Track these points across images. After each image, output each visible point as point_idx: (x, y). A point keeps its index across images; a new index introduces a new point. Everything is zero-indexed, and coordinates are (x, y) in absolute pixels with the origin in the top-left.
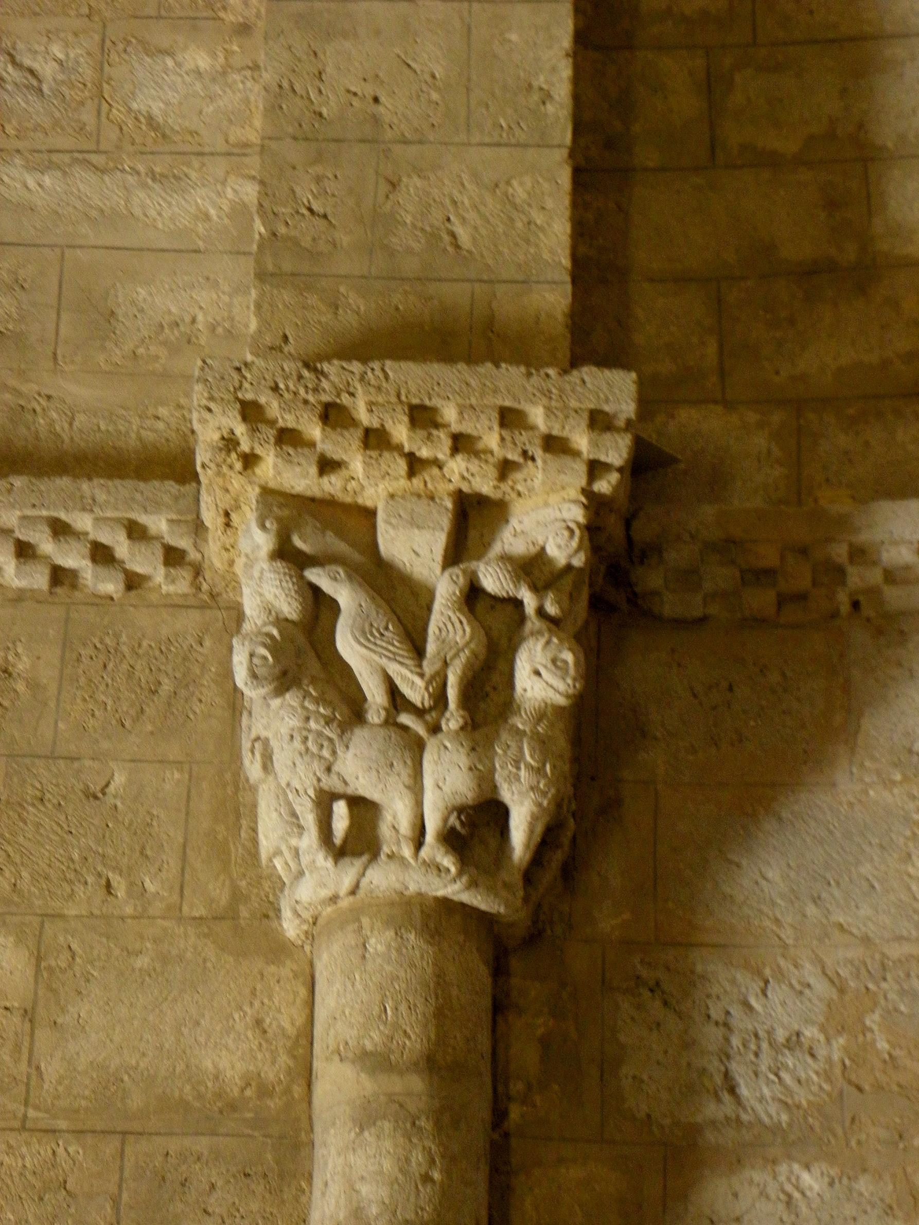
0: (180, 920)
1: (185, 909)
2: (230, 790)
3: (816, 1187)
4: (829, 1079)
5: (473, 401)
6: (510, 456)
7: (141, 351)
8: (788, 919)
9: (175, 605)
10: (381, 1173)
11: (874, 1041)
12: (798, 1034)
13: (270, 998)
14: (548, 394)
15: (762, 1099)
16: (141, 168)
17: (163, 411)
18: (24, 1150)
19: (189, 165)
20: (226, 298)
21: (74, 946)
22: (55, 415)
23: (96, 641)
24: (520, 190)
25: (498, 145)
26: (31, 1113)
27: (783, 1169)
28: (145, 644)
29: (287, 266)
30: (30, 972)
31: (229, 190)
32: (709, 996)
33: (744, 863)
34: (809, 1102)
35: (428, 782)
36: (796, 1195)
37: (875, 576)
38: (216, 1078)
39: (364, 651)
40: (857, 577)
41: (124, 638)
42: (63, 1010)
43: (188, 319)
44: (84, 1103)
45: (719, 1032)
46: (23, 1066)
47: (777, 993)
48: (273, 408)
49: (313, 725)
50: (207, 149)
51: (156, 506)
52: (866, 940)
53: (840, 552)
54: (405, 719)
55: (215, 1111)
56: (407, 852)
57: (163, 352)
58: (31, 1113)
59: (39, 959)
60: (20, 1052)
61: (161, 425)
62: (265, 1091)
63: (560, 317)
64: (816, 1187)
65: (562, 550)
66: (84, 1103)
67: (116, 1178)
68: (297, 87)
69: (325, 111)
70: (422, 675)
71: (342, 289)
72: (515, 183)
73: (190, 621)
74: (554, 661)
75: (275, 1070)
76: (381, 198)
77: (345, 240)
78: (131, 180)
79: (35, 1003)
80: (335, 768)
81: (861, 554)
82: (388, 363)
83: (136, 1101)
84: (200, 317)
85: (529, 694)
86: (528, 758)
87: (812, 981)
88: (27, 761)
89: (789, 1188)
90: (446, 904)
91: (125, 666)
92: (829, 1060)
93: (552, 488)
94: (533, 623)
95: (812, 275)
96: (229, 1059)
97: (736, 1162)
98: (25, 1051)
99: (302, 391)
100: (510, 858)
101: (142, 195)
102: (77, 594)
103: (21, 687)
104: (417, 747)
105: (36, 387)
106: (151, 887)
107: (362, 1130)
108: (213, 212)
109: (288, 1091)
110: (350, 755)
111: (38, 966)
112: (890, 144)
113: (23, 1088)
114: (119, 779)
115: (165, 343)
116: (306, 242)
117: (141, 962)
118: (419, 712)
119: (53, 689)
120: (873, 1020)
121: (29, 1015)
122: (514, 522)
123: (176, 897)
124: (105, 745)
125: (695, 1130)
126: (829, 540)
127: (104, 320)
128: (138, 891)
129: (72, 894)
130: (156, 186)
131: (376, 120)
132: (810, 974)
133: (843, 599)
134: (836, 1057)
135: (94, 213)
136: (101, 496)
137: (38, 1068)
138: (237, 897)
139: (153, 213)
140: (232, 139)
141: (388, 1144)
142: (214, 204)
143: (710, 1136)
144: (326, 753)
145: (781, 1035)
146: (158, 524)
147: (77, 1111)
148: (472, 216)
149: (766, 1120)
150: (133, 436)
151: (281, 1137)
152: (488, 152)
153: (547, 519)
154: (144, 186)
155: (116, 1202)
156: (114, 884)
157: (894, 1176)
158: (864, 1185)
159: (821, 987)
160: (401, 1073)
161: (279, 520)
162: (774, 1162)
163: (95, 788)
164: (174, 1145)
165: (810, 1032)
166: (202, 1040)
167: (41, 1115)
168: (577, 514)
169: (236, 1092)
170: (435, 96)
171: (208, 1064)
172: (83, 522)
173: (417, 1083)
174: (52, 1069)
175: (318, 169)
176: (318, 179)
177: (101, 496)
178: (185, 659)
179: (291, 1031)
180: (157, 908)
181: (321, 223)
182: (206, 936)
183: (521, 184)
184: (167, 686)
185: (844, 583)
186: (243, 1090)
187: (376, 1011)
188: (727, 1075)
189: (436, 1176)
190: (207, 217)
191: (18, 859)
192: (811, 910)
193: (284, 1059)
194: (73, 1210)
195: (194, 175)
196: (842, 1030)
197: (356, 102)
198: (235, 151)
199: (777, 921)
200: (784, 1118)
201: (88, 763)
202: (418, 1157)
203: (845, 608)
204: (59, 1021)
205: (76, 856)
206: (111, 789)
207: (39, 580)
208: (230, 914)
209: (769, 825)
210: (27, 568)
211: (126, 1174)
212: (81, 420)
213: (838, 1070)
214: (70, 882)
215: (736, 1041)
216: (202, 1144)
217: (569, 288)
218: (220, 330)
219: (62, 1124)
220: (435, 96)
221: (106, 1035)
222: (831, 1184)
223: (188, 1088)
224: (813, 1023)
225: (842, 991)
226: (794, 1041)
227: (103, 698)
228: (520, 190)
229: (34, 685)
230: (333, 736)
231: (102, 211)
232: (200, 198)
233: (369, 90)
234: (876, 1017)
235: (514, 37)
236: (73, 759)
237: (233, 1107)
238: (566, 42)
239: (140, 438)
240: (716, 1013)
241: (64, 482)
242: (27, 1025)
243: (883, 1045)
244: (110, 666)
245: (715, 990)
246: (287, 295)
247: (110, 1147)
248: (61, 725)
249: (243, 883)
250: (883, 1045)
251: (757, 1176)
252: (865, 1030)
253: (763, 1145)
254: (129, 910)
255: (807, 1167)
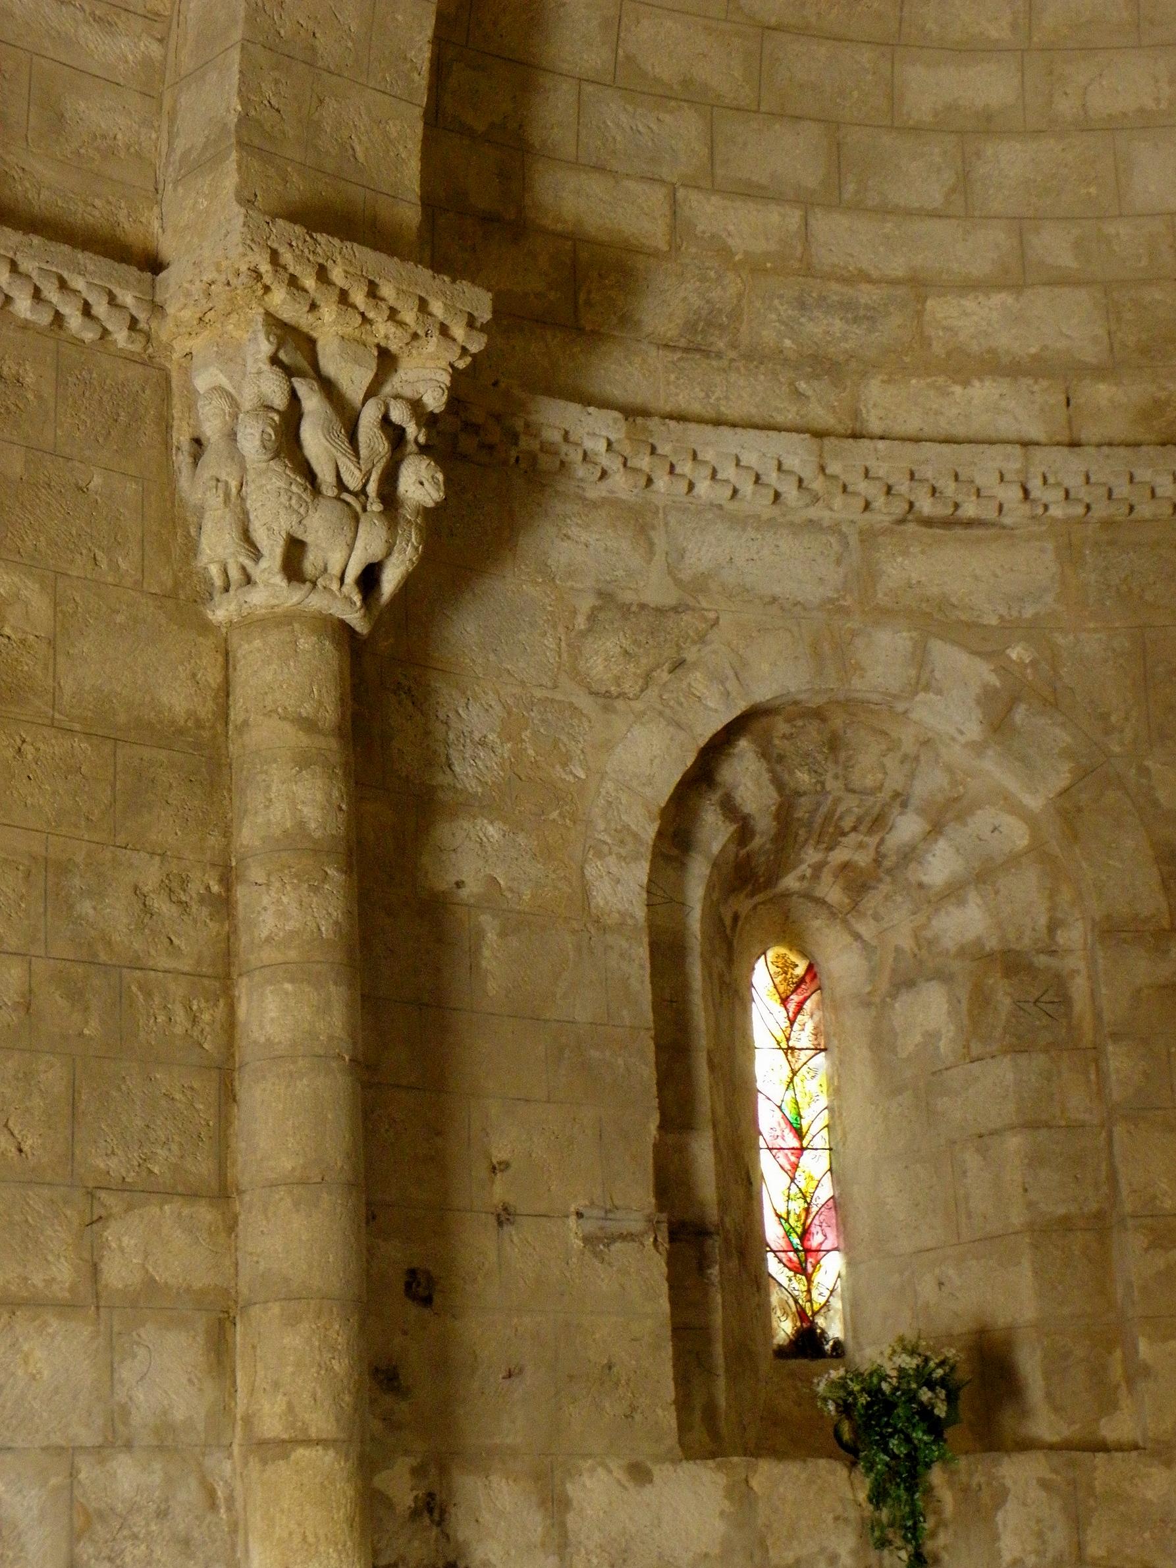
0: (142, 592)
1: (145, 585)
2: (169, 505)
3: (496, 836)
4: (503, 770)
5: (404, 288)
6: (419, 332)
7: (82, 151)
8: (480, 661)
9: (129, 358)
10: (314, 800)
11: (525, 750)
12: (485, 737)
13: (200, 659)
14: (444, 294)
15: (467, 775)
16: (86, 7)
17: (97, 202)
18: (53, 741)
19: (119, 16)
20: (137, 127)
21: (77, 599)
22: (28, 185)
23: (77, 372)
24: (393, 130)
25: (384, 93)
26: (57, 716)
27: (478, 821)
28: (108, 382)
29: (257, 142)
30: (50, 612)
31: (142, 44)
32: (438, 703)
33: (455, 618)
34: (493, 782)
35: (359, 544)
36: (485, 839)
37: (536, 446)
38: (170, 709)
39: (327, 444)
40: (525, 443)
41: (94, 375)
42: (73, 645)
43: (111, 135)
44: (90, 714)
45: (444, 728)
46: (50, 681)
47: (475, 708)
48: (287, 257)
49: (294, 488)
50: (131, 8)
51: (126, 285)
52: (522, 683)
53: (519, 425)
54: (345, 496)
55: (161, 732)
56: (335, 586)
57: (97, 157)
58: (57, 716)
59: (56, 605)
60: (47, 669)
61: (97, 213)
62: (199, 724)
63: (415, 229)
64: (496, 836)
65: (434, 401)
66: (90, 714)
67: (112, 771)
68: (267, 8)
69: (282, 32)
70: (360, 470)
71: (289, 169)
72: (391, 123)
73: (135, 372)
74: (433, 477)
75: (206, 710)
76: (313, 110)
77: (291, 133)
78: (80, 15)
79: (55, 635)
80: (304, 522)
81: (532, 430)
82: (355, 245)
83: (122, 718)
84: (119, 136)
85: (409, 495)
86: (413, 540)
87: (493, 703)
88: (40, 454)
89: (481, 835)
90: (344, 626)
91: (96, 396)
92: (502, 757)
93: (433, 357)
94: (412, 447)
95: (488, 219)
96: (178, 699)
97: (454, 816)
98: (51, 669)
99: (306, 251)
100: (378, 599)
101: (86, 29)
102: (62, 333)
103: (30, 396)
104: (356, 519)
105: (15, 160)
106: (124, 566)
107: (301, 769)
108: (130, 57)
109: (213, 727)
110: (317, 515)
111: (55, 608)
112: (536, 144)
113: (50, 696)
114: (97, 481)
115: (97, 149)
116: (267, 127)
117: (120, 619)
118: (355, 494)
119: (51, 404)
120: (526, 735)
121: (51, 643)
122: (401, 372)
123: (139, 576)
124: (87, 453)
125: (432, 790)
126: (514, 415)
127: (58, 123)
128: (114, 567)
129: (72, 561)
130: (96, 25)
131: (313, 49)
132: (491, 699)
133: (514, 453)
134: (506, 756)
135: (53, 33)
136: (91, 268)
137: (59, 683)
138: (177, 584)
139: (92, 46)
140: (148, 6)
141: (319, 783)
142: (132, 52)
143: (440, 795)
144: (302, 510)
145: (477, 736)
146: (127, 298)
147: (85, 719)
148: (364, 138)
149: (470, 790)
150: (80, 216)
151: (211, 758)
152: (378, 95)
153: (426, 378)
154: (88, 22)
155: (113, 787)
156: (99, 558)
157: (538, 836)
158: (521, 839)
159: (498, 708)
160: (325, 735)
161: (278, 337)
162: (475, 817)
163: (82, 484)
164: (147, 753)
165: (492, 737)
166: (160, 681)
167: (62, 717)
168: (446, 379)
169: (182, 723)
170: (350, 44)
171: (165, 699)
172: (78, 283)
173: (334, 743)
174: (68, 685)
175: (276, 74)
176: (277, 82)
177: (91, 268)
178: (134, 400)
179: (214, 685)
180: (128, 581)
181: (276, 114)
182: (160, 608)
183: (395, 125)
184: (123, 418)
185: (516, 444)
186: (186, 721)
187: (307, 690)
188: (448, 757)
189: (344, 807)
190: (127, 62)
191: (36, 527)
192: (492, 657)
193: (210, 704)
194: (87, 789)
195: (120, 24)
196: (509, 740)
197: (302, 32)
198: (149, 15)
199: (473, 661)
200: (480, 790)
201: (78, 464)
202: (336, 794)
203: (513, 460)
204: (71, 652)
205: (74, 532)
206: (91, 486)
207: (45, 318)
208: (172, 595)
209: (468, 596)
210: (38, 307)
211: (118, 769)
212: (45, 194)
213: (507, 764)
214: (72, 552)
215: (451, 736)
216: (162, 755)
217: (420, 208)
218: (132, 150)
219: (77, 727)
220: (350, 44)
221: (96, 669)
222: (504, 836)
223: (153, 714)
224: (494, 731)
225: (509, 713)
226: (482, 743)
227: (83, 417)
228: (393, 130)
229: (39, 397)
230: (309, 500)
231: (59, 33)
232: (123, 44)
233: (311, 25)
234: (528, 733)
235: (400, 17)
236: (69, 459)
237: (181, 732)
238: (429, 33)
239: (83, 219)
240: (442, 716)
241: (66, 248)
242: (52, 651)
243: (531, 752)
244: (87, 394)
245: (441, 700)
246: (256, 164)
247: (107, 748)
248: (59, 433)
249: (181, 574)
250: (531, 752)
251: (465, 825)
252: (522, 741)
253: (466, 806)
254: (110, 579)
255: (492, 823)
